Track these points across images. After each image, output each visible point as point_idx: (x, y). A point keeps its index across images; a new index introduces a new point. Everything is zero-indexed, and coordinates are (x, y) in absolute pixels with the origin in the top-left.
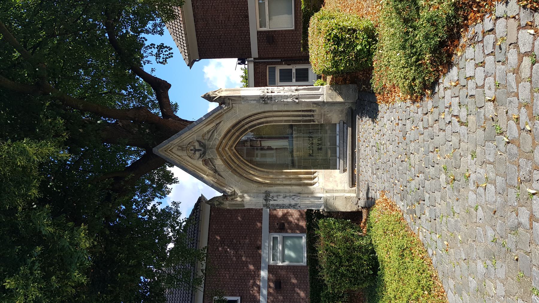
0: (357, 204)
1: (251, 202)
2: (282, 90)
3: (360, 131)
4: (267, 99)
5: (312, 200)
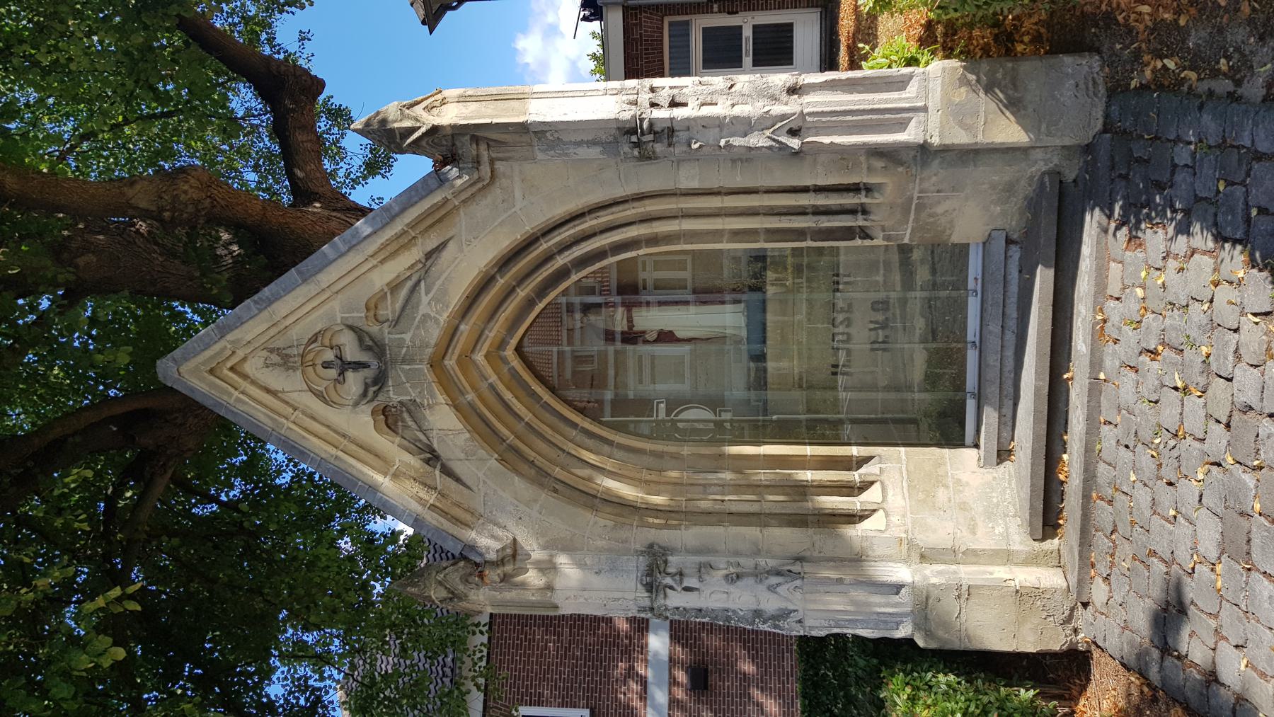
0: (1069, 619)
1: (586, 594)
2: (721, 93)
3: (1015, 252)
4: (650, 137)
5: (860, 595)
